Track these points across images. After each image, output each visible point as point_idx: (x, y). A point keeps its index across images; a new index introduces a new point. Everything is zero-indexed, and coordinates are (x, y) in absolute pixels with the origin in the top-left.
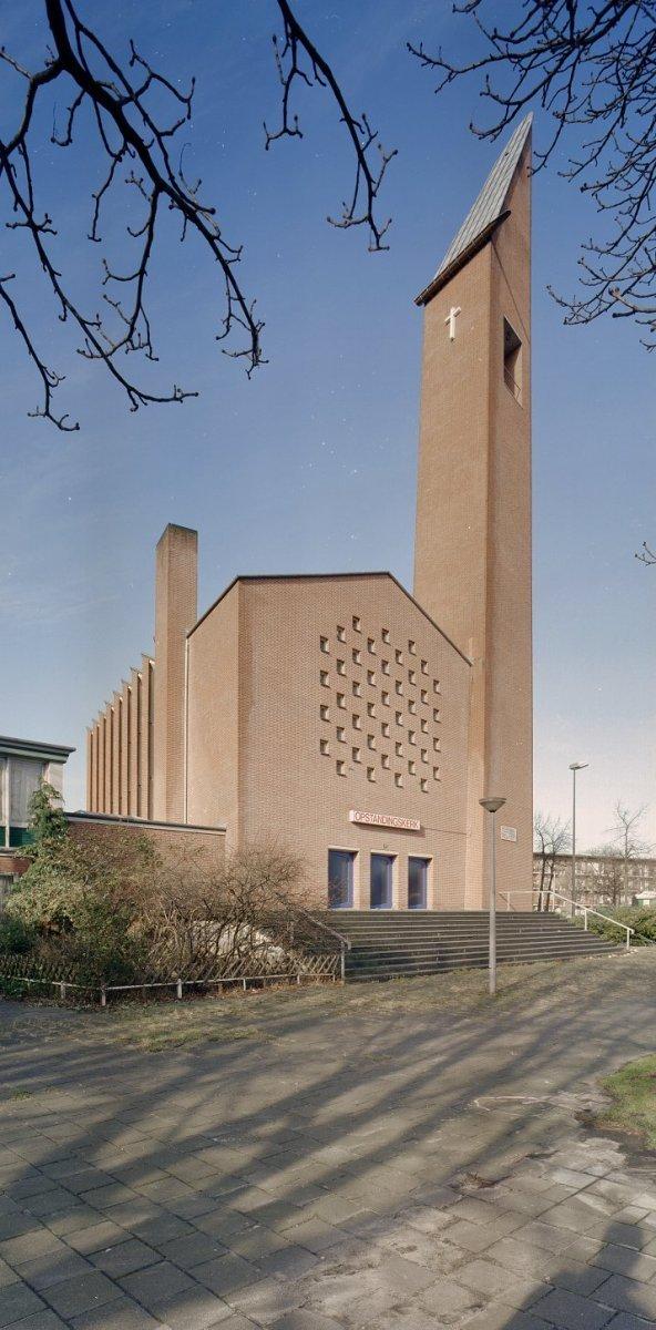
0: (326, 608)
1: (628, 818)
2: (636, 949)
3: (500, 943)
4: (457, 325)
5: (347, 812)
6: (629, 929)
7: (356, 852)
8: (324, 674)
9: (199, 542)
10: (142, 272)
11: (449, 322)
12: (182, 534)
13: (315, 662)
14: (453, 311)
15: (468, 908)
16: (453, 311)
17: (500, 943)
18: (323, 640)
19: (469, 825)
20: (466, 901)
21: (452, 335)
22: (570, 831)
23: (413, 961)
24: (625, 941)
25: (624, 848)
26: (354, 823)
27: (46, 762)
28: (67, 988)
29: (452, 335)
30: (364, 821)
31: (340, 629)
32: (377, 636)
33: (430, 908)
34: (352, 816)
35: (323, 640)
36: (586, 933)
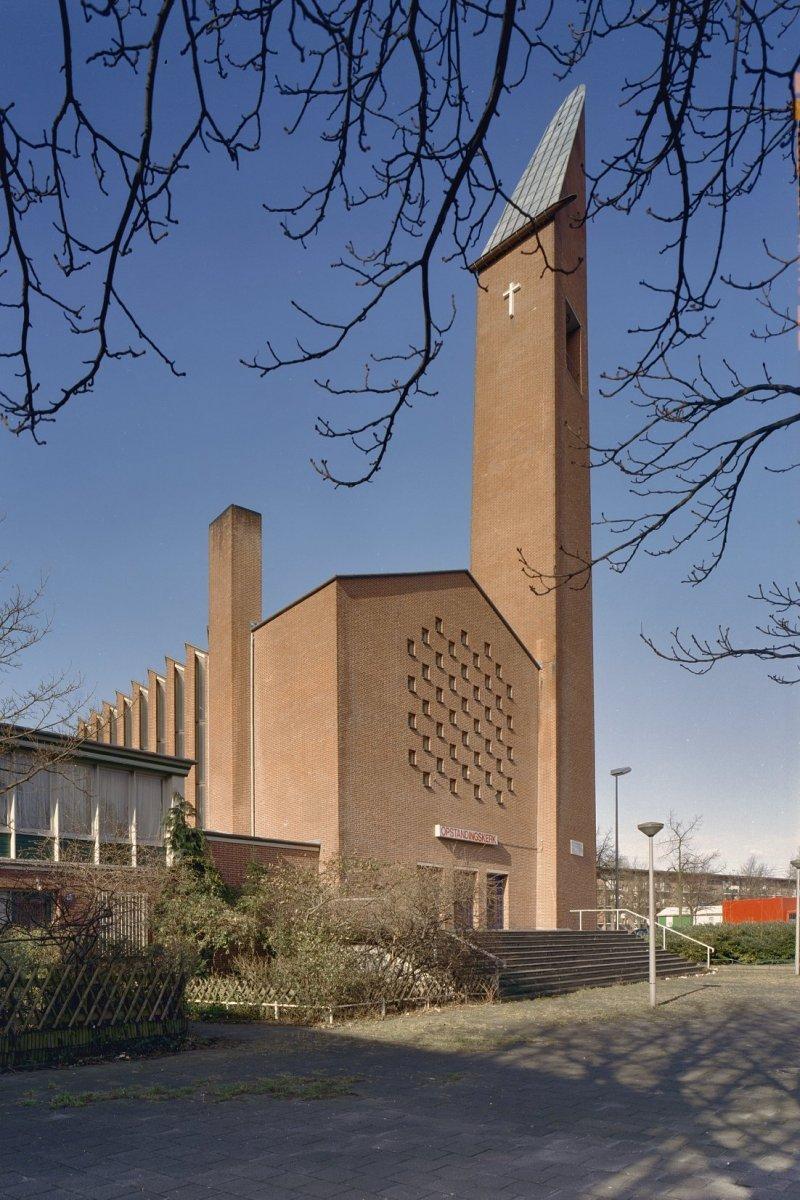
0: (416, 608)
1: (681, 831)
2: (716, 968)
3: (661, 957)
4: (516, 301)
5: (433, 827)
6: (709, 948)
7: (506, 875)
8: (411, 679)
9: (263, 523)
10: (604, 558)
11: (507, 297)
12: (246, 517)
13: (400, 668)
14: (512, 287)
15: (539, 928)
16: (512, 287)
17: (661, 957)
18: (411, 643)
19: (540, 839)
20: (539, 920)
21: (511, 312)
22: (612, 842)
23: (555, 980)
24: (705, 961)
25: (678, 862)
26: (439, 838)
27: (169, 775)
28: (280, 1008)
29: (511, 312)
30: (448, 836)
31: (425, 631)
32: (456, 637)
33: (506, 928)
34: (438, 831)
35: (411, 643)
36: (664, 952)
